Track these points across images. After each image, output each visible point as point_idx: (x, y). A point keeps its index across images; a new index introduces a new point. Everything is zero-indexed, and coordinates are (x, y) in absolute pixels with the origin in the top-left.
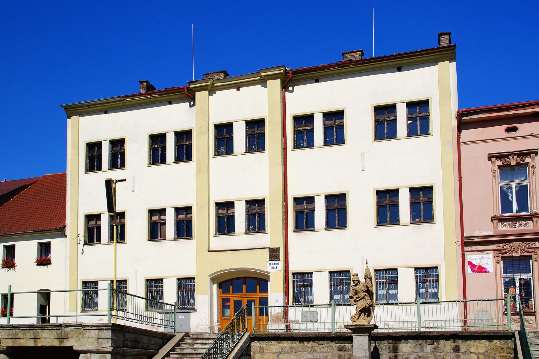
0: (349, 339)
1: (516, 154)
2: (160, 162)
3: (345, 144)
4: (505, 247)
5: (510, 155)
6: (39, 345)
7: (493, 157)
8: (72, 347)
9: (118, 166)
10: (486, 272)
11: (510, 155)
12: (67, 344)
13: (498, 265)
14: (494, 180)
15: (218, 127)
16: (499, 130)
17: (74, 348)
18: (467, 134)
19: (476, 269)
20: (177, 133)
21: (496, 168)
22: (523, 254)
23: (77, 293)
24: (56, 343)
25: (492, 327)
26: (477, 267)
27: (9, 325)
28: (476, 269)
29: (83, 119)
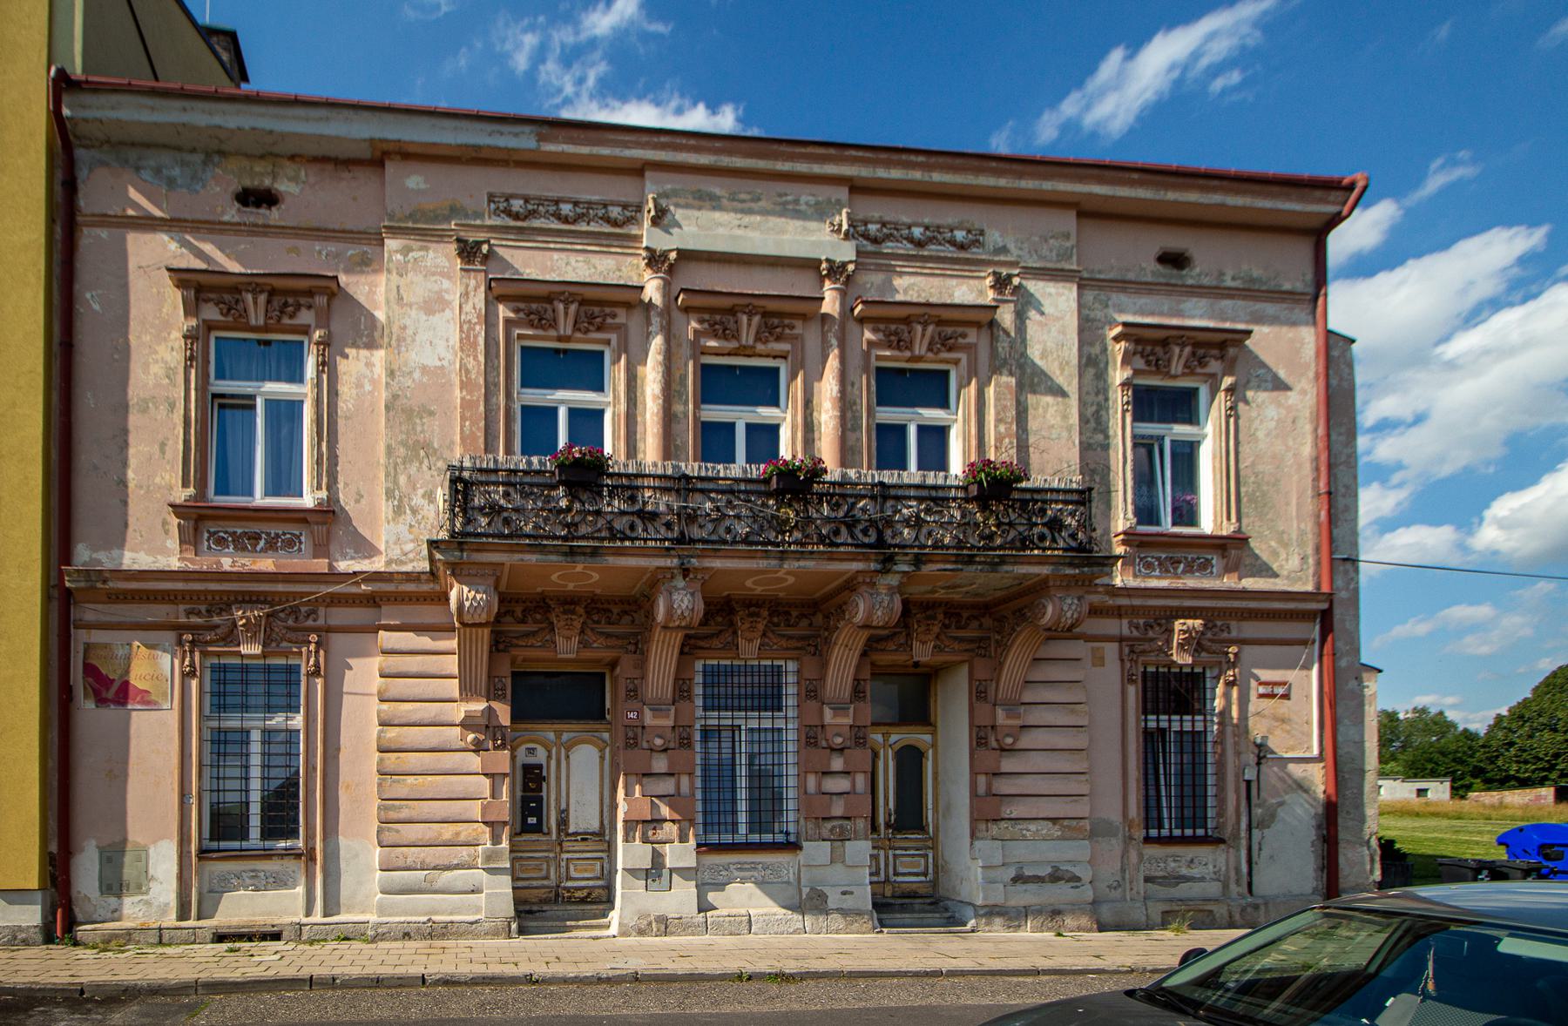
19: (111, 694)
28: (111, 694)
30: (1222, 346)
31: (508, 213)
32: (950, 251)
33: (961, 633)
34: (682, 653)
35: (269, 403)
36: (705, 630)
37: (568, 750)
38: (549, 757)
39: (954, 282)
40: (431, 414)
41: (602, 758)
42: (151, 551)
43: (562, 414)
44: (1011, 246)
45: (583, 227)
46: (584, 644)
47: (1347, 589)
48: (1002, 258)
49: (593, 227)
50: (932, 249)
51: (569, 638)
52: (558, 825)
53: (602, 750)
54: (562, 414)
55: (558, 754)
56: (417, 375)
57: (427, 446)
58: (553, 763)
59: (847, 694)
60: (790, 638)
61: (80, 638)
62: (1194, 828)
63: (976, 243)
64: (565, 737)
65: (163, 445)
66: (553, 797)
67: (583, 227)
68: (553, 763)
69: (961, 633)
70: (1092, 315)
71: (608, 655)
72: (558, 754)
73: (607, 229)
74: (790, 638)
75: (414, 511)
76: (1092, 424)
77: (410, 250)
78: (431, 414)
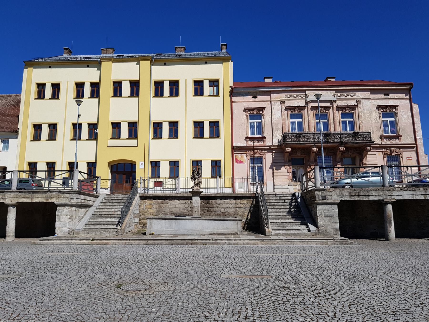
0: (191, 198)
1: (390, 107)
2: (174, 95)
3: (179, 96)
4: (251, 152)
5: (388, 107)
6: (34, 202)
7: (247, 109)
8: (4, 202)
9: (173, 95)
10: (243, 163)
11: (388, 107)
12: (50, 201)
13: (248, 160)
14: (380, 118)
15: (114, 83)
16: (250, 98)
17: (55, 203)
18: (234, 99)
19: (238, 162)
20: (131, 81)
21: (248, 115)
22: (259, 156)
23: (62, 168)
24: (44, 201)
25: (336, 194)
26: (239, 161)
27: (233, 195)
28: (238, 162)
29: (35, 70)
30: (262, 109)
31: (287, 97)
32: (350, 97)
33: (305, 152)
34: (315, 155)
35: (298, 122)
36: (319, 152)
37: (299, 169)
38: (296, 170)
39: (352, 101)
40: (279, 124)
41: (304, 170)
42: (243, 143)
43: (389, 121)
44: (360, 95)
45: (297, 98)
46: (301, 154)
47: (421, 142)
48: (359, 97)
49: (299, 98)
50: (348, 97)
51: (299, 153)
52: (298, 180)
53: (304, 169)
54: (389, 121)
55: (298, 170)
56: (276, 119)
57: (278, 128)
58: (297, 171)
59: (314, 161)
60: (331, 153)
61: (235, 155)
62: (254, 182)
63: (355, 96)
64: (298, 167)
65: (244, 130)
66: (297, 176)
67: (297, 98)
68: (297, 171)
69: (305, 152)
70: (374, 104)
71: (304, 156)
72: (298, 170)
73: (294, 98)
74: (331, 153)
75: (277, 137)
76: (375, 120)
77: (275, 103)
78: (279, 124)
